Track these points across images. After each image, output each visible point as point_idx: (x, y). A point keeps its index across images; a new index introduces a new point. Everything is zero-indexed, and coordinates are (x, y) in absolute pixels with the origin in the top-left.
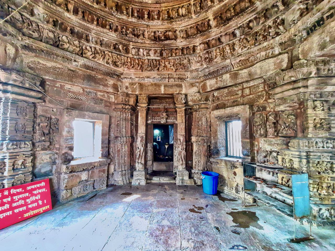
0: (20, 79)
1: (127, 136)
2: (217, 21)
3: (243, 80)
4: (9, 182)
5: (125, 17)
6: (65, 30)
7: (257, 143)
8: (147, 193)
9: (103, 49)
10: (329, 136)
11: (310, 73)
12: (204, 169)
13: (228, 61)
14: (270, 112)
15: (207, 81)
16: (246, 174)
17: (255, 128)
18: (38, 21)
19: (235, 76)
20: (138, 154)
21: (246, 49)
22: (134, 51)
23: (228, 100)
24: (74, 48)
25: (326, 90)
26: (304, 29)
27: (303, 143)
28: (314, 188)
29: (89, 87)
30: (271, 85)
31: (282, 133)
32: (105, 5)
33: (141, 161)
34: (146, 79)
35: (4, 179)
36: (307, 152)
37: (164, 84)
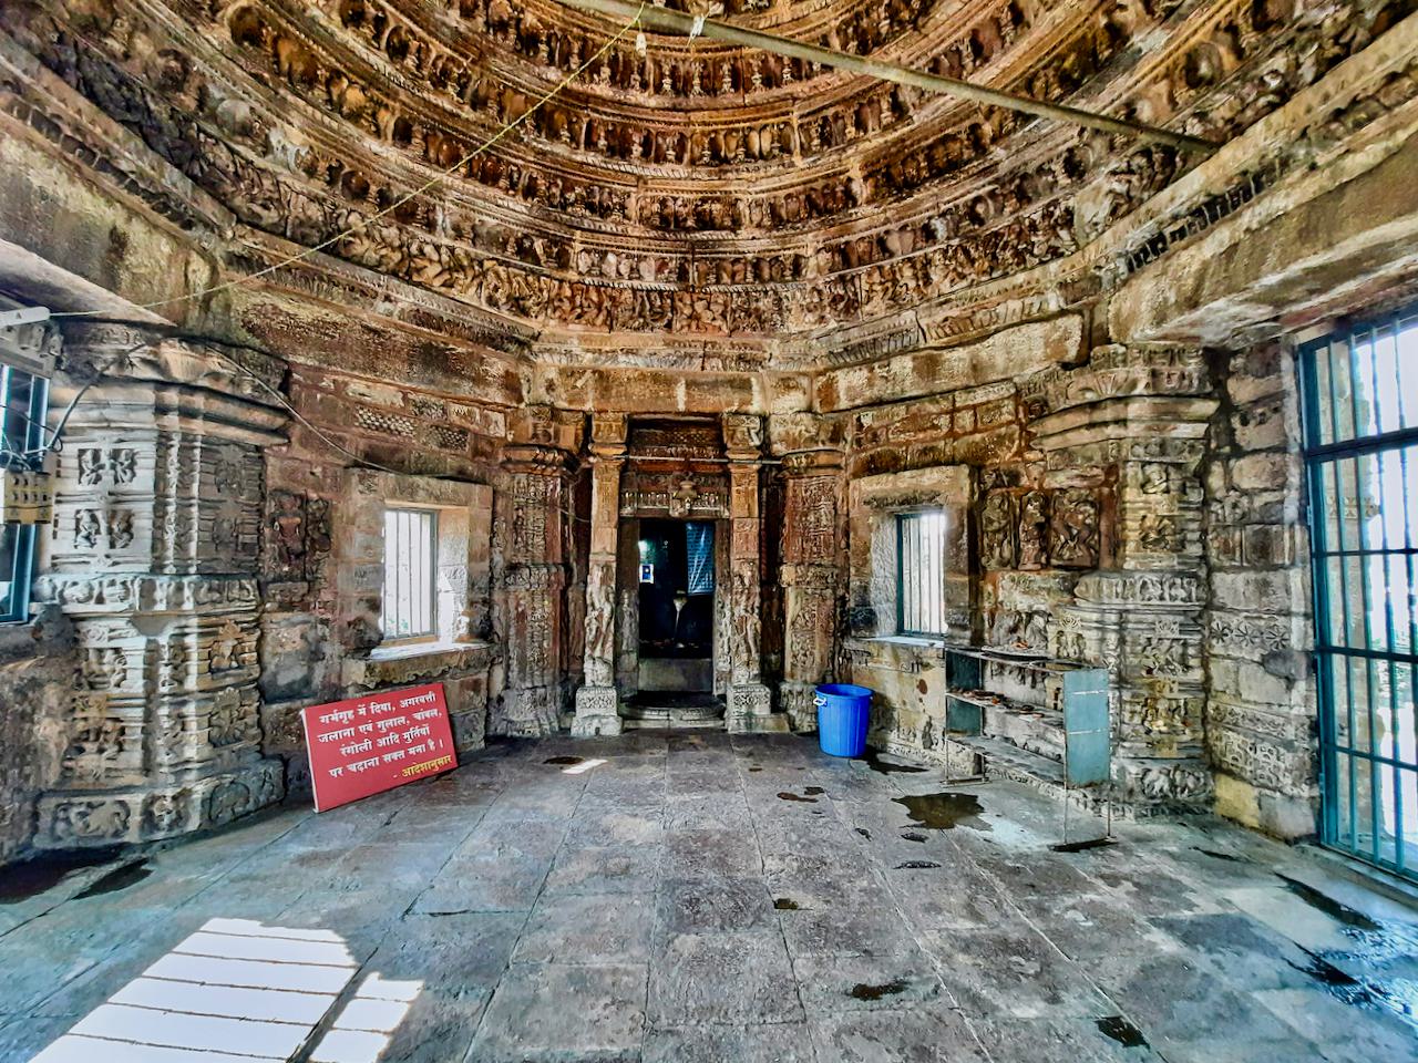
0: (229, 369)
1: (550, 561)
2: (876, 186)
3: (952, 384)
4: (203, 712)
5: (561, 149)
6: (360, 193)
7: (990, 588)
8: (633, 757)
9: (480, 252)
10: (1178, 568)
11: (1134, 384)
12: (824, 678)
13: (908, 315)
14: (1031, 489)
15: (839, 374)
16: (955, 684)
17: (986, 541)
18: (279, 169)
19: (929, 366)
20: (594, 627)
21: (965, 283)
22: (583, 262)
23: (908, 443)
24: (384, 252)
25: (1174, 434)
26: (1120, 255)
27: (1111, 585)
28: (1133, 712)
29: (423, 387)
30: (1034, 407)
31: (1060, 556)
32: (501, 111)
33: (603, 651)
34: (622, 358)
35: (184, 703)
36: (1121, 613)
37: (686, 375)
